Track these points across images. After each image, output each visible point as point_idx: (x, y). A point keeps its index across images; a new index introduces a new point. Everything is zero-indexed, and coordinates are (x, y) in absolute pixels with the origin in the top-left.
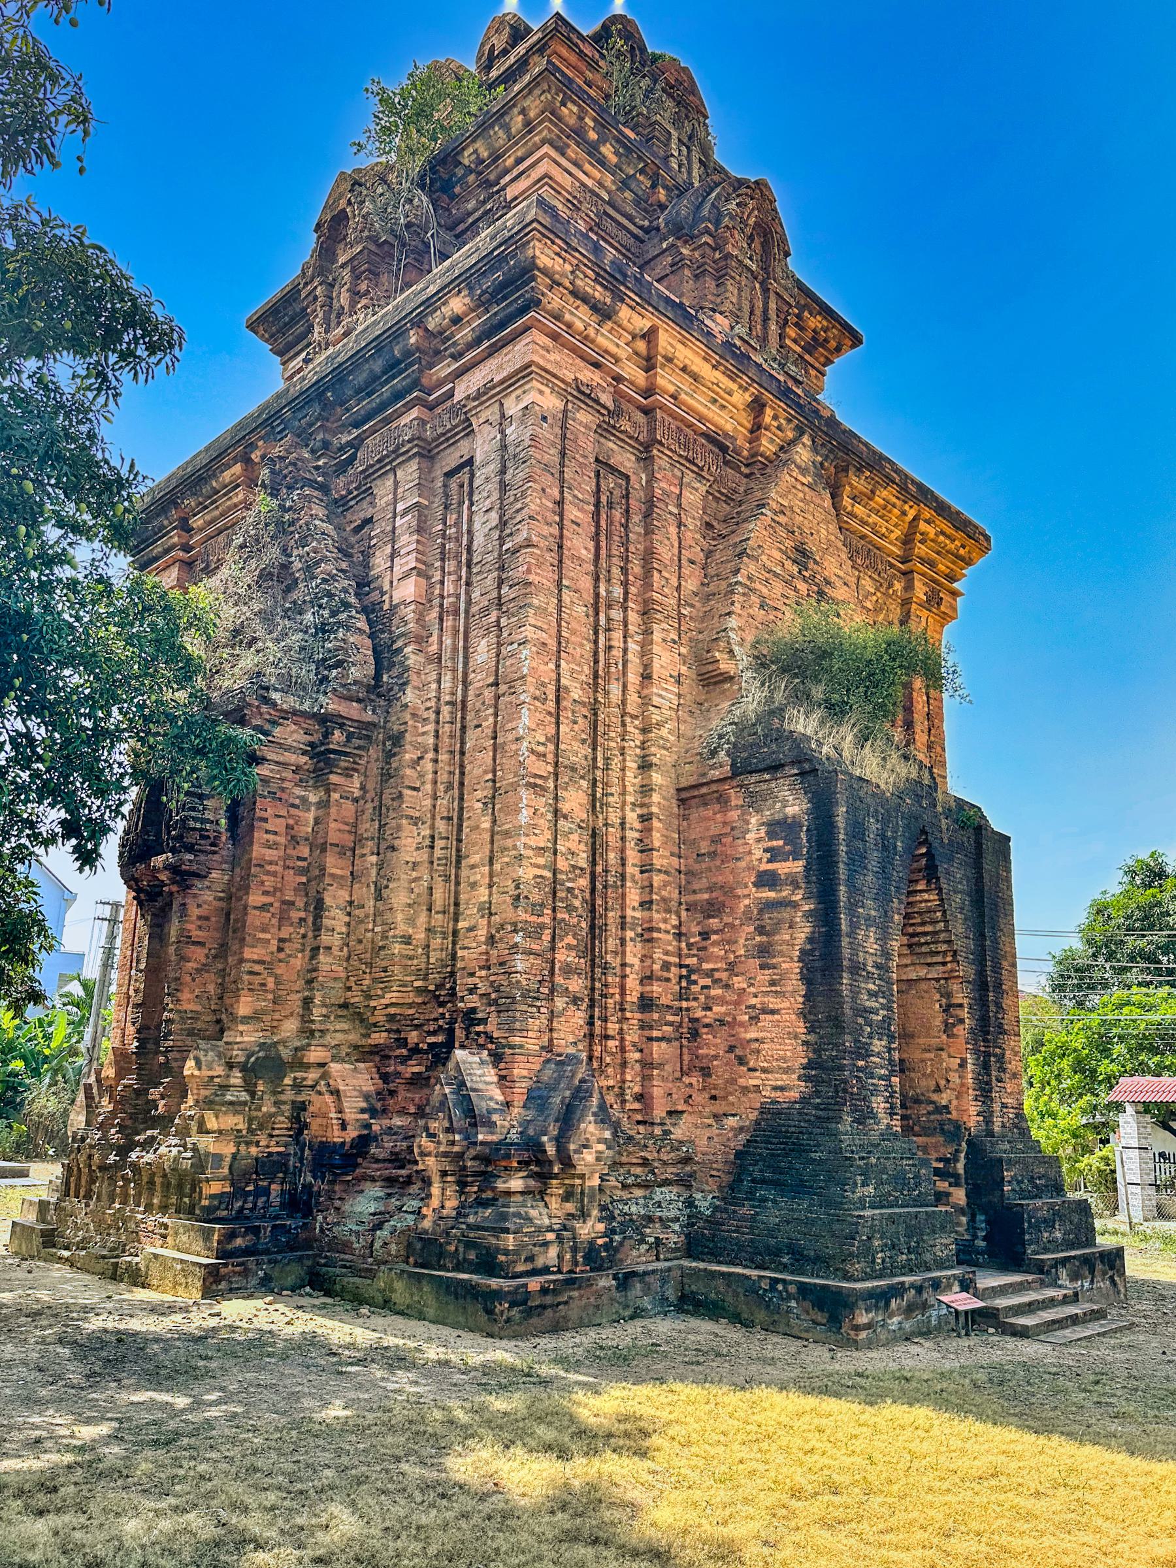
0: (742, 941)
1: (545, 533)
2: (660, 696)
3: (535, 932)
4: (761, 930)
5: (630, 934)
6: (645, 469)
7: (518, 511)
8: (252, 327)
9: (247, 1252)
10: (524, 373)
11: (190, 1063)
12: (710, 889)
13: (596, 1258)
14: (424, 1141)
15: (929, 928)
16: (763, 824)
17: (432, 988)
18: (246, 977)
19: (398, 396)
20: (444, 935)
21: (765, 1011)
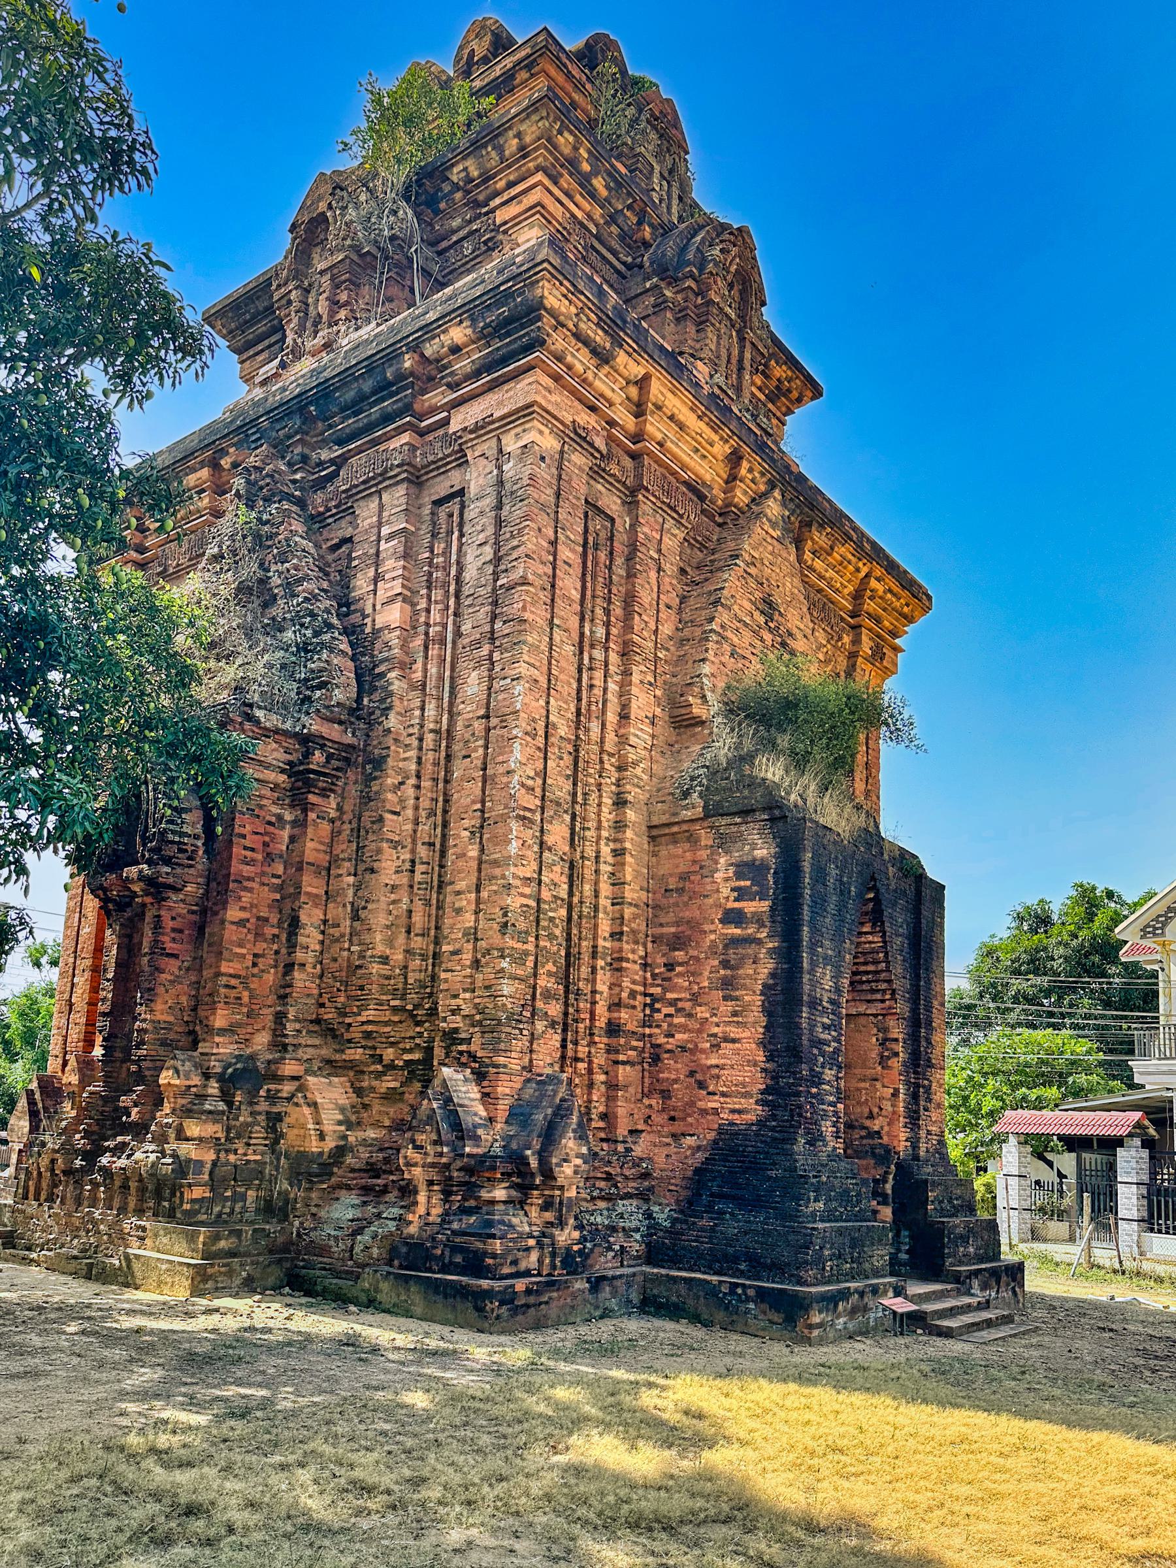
0: (706, 973)
1: (540, 572)
3: (520, 959)
4: (725, 964)
5: (600, 963)
6: (629, 513)
7: (514, 548)
9: (232, 1254)
10: (525, 412)
12: (677, 924)
13: (573, 1262)
15: (871, 968)
17: (410, 1007)
18: (222, 990)
20: (424, 957)
21: (726, 1039)
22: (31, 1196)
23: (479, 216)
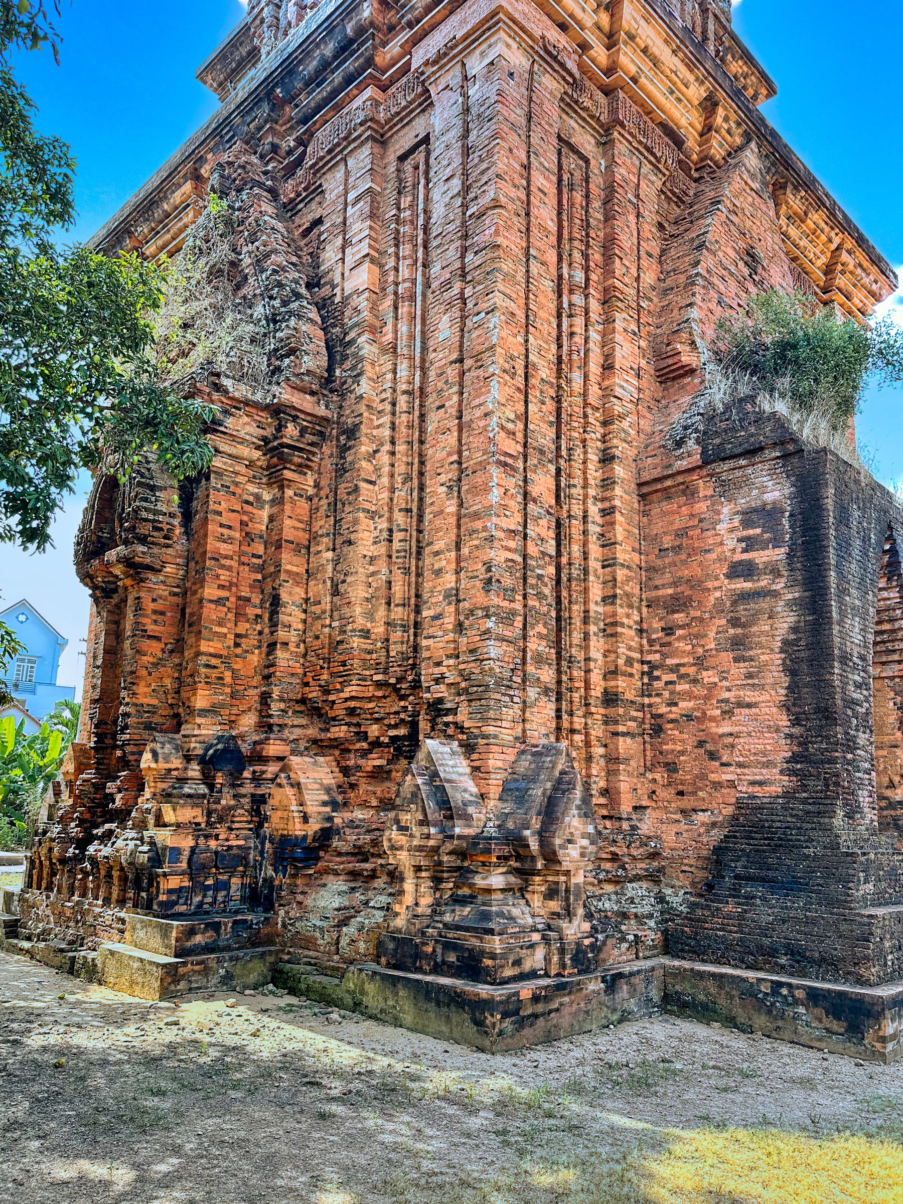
0: (712, 635)
2: (622, 387)
3: (507, 618)
6: (604, 155)
7: (483, 173)
8: (201, 77)
9: (208, 949)
11: (147, 756)
12: (674, 584)
13: (584, 959)
14: (395, 834)
16: (737, 513)
17: (393, 681)
18: (203, 670)
19: (349, 80)
21: (740, 705)
22: (34, 886)
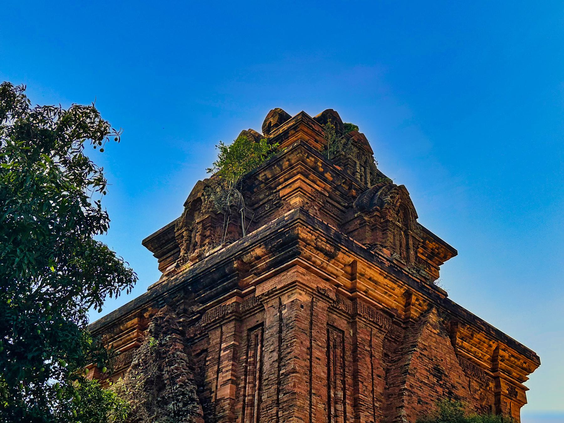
1: (303, 365)
6: (352, 327)
7: (289, 353)
8: (146, 243)
10: (293, 285)
23: (272, 193)
